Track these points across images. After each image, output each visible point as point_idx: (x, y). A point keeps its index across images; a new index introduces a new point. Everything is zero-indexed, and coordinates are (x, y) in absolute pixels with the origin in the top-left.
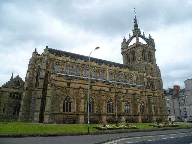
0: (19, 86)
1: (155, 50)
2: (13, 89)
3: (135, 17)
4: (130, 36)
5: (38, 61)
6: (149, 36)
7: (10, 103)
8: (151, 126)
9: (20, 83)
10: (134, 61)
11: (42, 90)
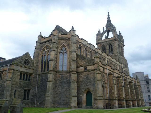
0: (29, 65)
1: (124, 46)
2: (23, 68)
3: (108, 14)
4: (104, 29)
5: (62, 41)
6: (98, 31)
7: (21, 85)
8: (142, 111)
9: (30, 62)
11: (76, 73)
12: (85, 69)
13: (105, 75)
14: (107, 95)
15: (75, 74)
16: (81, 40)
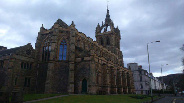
3: (108, 9)
4: (103, 23)
7: (22, 73)
10: (108, 45)
12: (83, 59)
13: (100, 65)
14: (101, 82)
15: (74, 63)
16: (80, 34)
